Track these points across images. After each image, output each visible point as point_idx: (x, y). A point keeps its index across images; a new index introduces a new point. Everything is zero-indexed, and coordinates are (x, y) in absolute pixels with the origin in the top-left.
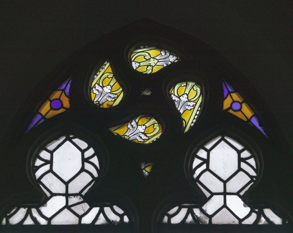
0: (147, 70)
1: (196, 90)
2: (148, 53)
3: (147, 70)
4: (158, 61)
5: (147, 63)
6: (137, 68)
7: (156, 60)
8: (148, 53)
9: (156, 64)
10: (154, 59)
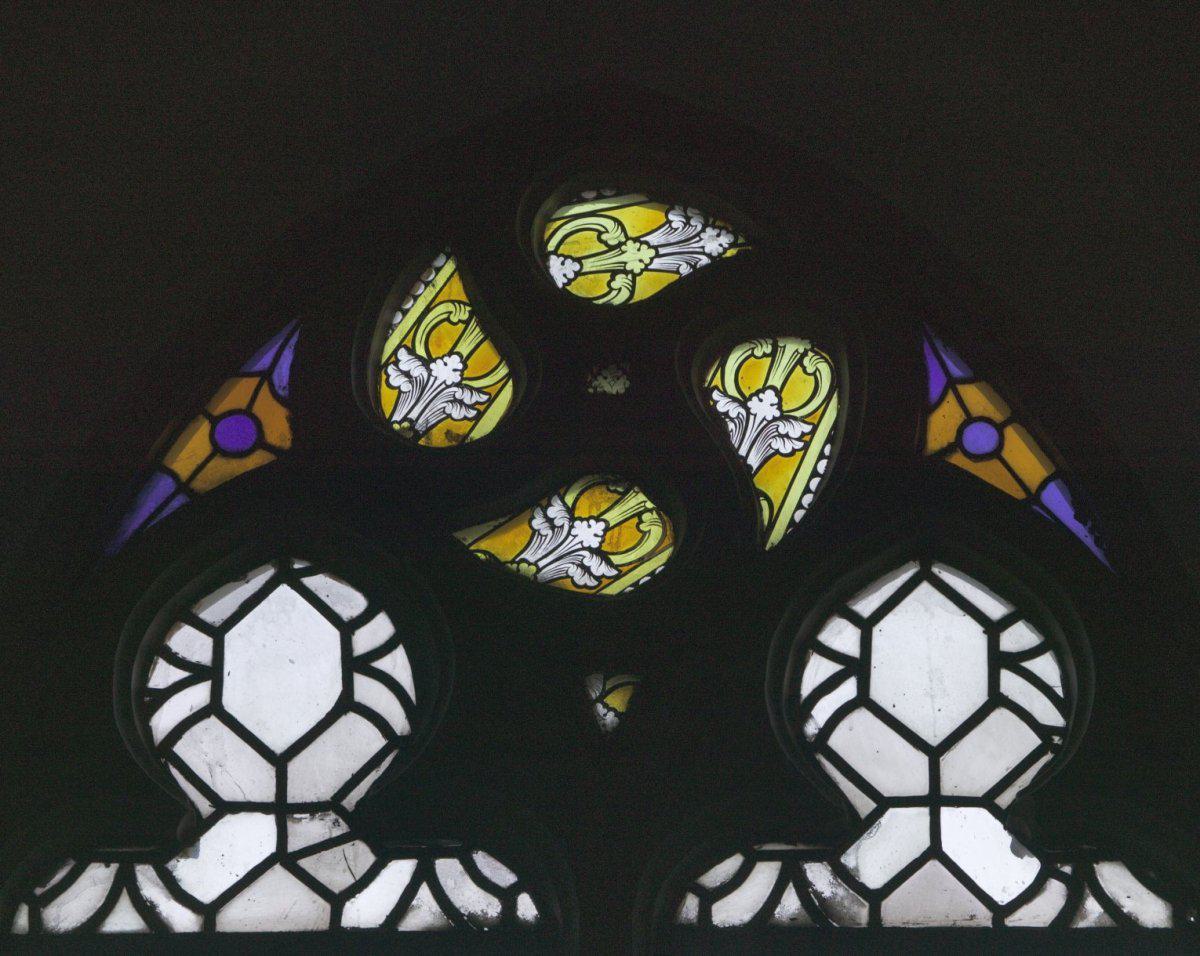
0: (611, 289)
1: (814, 374)
2: (616, 220)
3: (611, 289)
4: (657, 252)
5: (610, 261)
6: (570, 281)
7: (650, 247)
8: (616, 220)
9: (647, 265)
10: (638, 245)
